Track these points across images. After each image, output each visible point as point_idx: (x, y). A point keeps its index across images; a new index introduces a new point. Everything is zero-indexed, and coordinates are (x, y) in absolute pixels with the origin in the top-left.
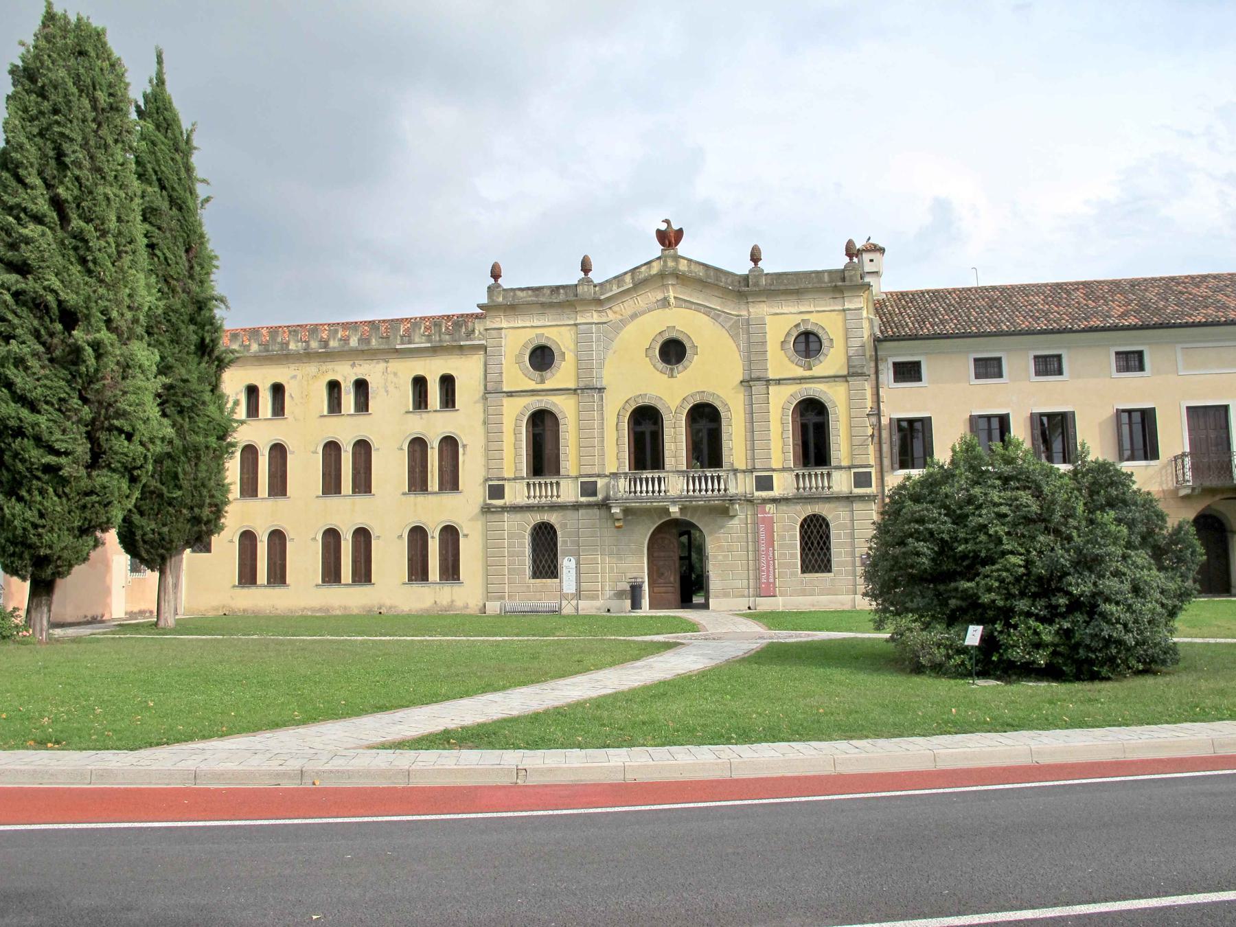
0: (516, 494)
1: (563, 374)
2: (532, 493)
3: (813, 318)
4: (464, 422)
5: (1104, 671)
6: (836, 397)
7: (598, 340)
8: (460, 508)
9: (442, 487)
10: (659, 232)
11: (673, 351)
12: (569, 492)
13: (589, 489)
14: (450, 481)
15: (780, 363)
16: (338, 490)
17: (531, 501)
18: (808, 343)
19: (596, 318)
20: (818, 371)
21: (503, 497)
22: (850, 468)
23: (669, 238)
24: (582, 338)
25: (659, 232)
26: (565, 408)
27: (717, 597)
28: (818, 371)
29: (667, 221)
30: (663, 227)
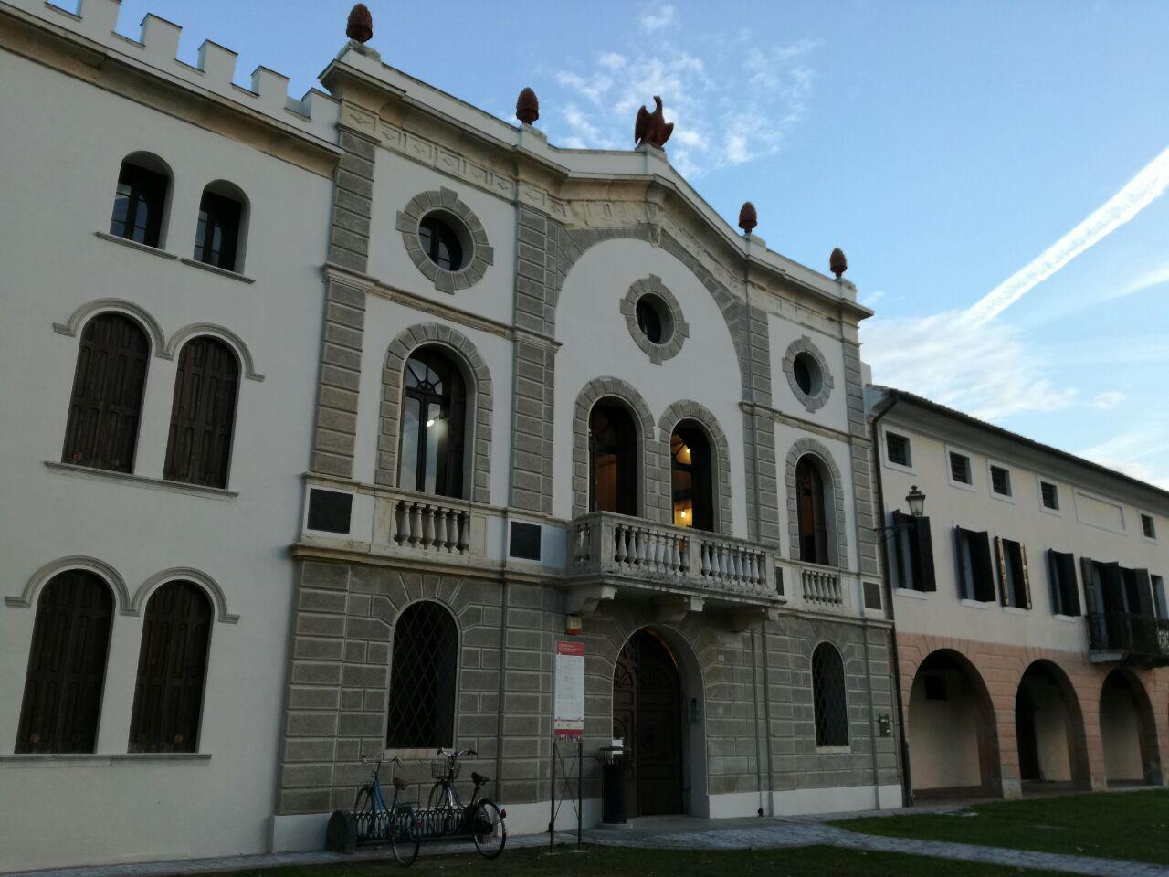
0: (370, 525)
1: (490, 293)
2: (408, 532)
3: (467, 196)
4: (272, 310)
5: (814, 820)
6: (839, 456)
7: (551, 250)
8: (236, 540)
9: (177, 471)
10: (643, 112)
11: (653, 317)
12: (488, 542)
13: (525, 541)
14: (203, 457)
15: (391, 255)
16: (120, 459)
17: (406, 551)
18: (446, 238)
19: (546, 207)
20: (462, 299)
21: (345, 528)
22: (504, 513)
23: (652, 129)
24: (531, 230)
25: (643, 112)
26: (494, 359)
27: (718, 791)
28: (462, 299)
29: (658, 100)
30: (651, 109)
